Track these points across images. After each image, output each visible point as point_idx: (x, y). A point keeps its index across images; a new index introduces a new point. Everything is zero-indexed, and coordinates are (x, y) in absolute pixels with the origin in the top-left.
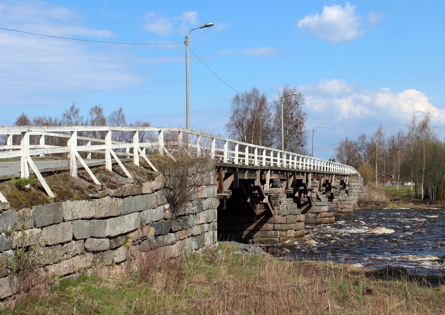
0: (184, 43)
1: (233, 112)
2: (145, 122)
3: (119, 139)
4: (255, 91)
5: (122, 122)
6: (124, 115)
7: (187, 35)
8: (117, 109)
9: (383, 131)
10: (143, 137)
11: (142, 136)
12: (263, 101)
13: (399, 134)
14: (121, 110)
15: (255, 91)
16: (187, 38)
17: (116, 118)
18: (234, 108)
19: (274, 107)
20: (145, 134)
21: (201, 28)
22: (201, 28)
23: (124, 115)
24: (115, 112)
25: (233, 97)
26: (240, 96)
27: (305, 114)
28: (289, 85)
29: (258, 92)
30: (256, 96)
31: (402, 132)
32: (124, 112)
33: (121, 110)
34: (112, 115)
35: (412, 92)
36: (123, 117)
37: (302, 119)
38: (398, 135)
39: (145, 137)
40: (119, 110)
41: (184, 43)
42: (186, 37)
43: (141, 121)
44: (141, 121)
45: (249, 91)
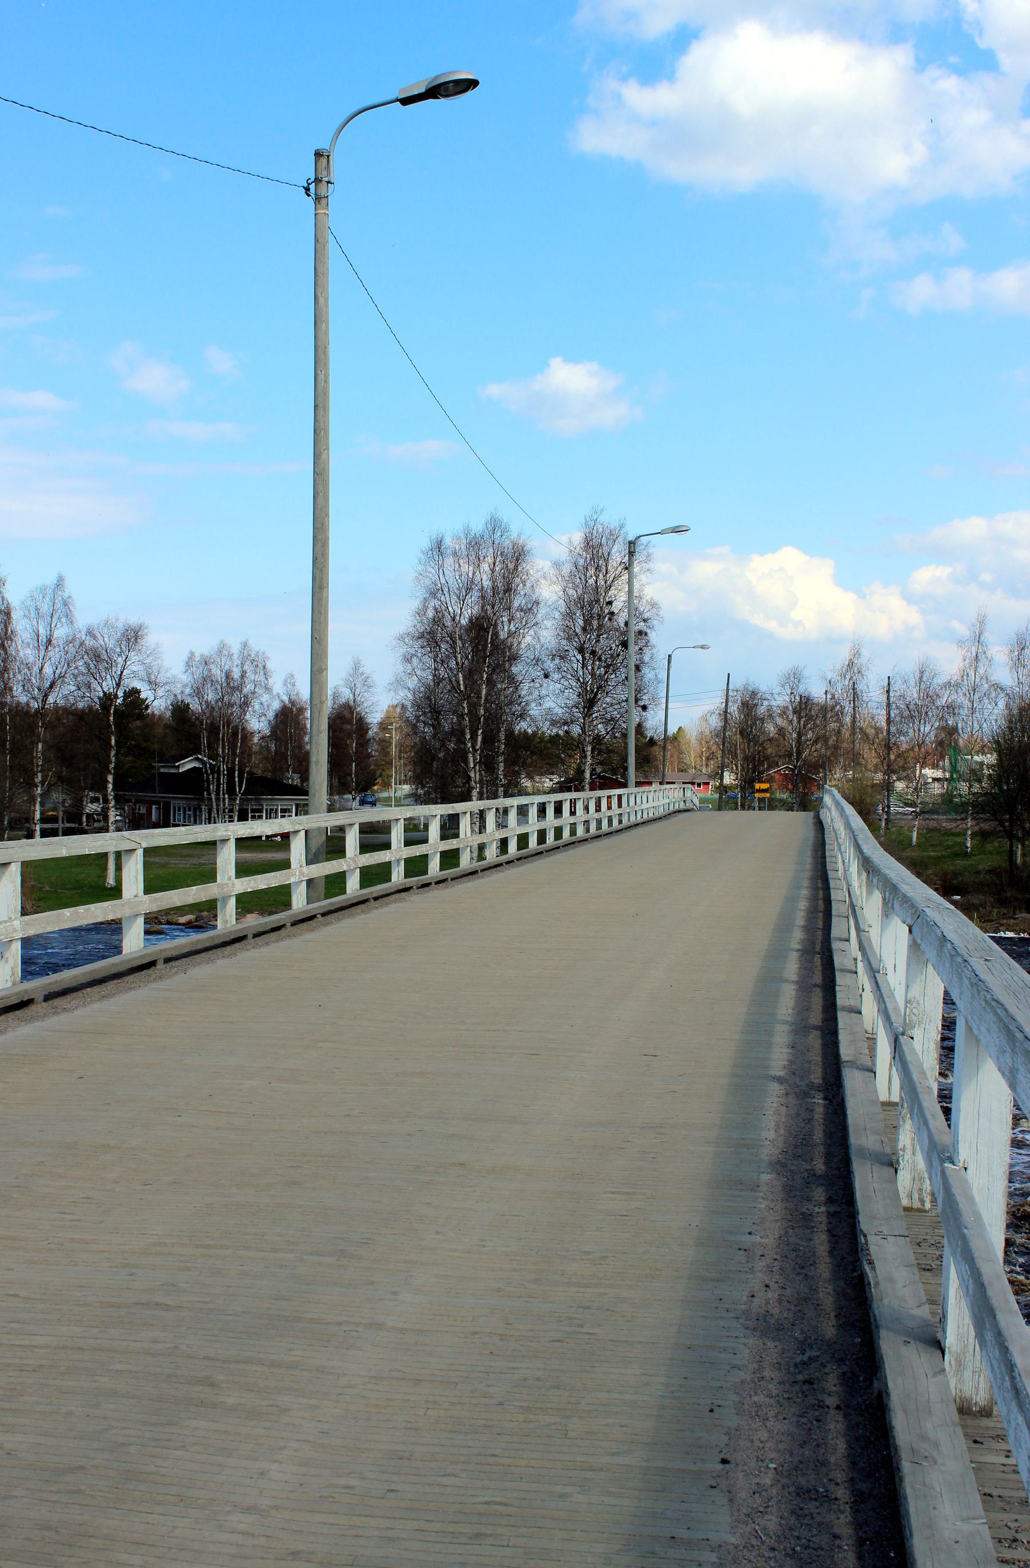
0: (307, 189)
1: (421, 594)
2: (131, 622)
3: (54, 673)
4: (495, 525)
5: (64, 620)
6: (69, 597)
7: (324, 145)
8: (51, 580)
9: (863, 660)
10: (122, 672)
11: (119, 669)
12: (518, 555)
13: (922, 672)
14: (60, 583)
15: (495, 525)
16: (324, 161)
17: (45, 608)
18: (428, 582)
19: (555, 579)
20: (128, 663)
21: (406, 101)
22: (406, 101)
23: (69, 597)
24: (43, 589)
25: (426, 544)
26: (448, 541)
27: (653, 605)
28: (602, 510)
29: (505, 530)
30: (496, 542)
31: (931, 667)
32: (71, 588)
33: (60, 583)
34: (33, 598)
35: (790, 557)
36: (65, 604)
37: (645, 621)
38: (917, 676)
39: (129, 672)
40: (55, 582)
41: (307, 189)
42: (318, 155)
43: (117, 620)
44: (117, 620)
45: (478, 526)
